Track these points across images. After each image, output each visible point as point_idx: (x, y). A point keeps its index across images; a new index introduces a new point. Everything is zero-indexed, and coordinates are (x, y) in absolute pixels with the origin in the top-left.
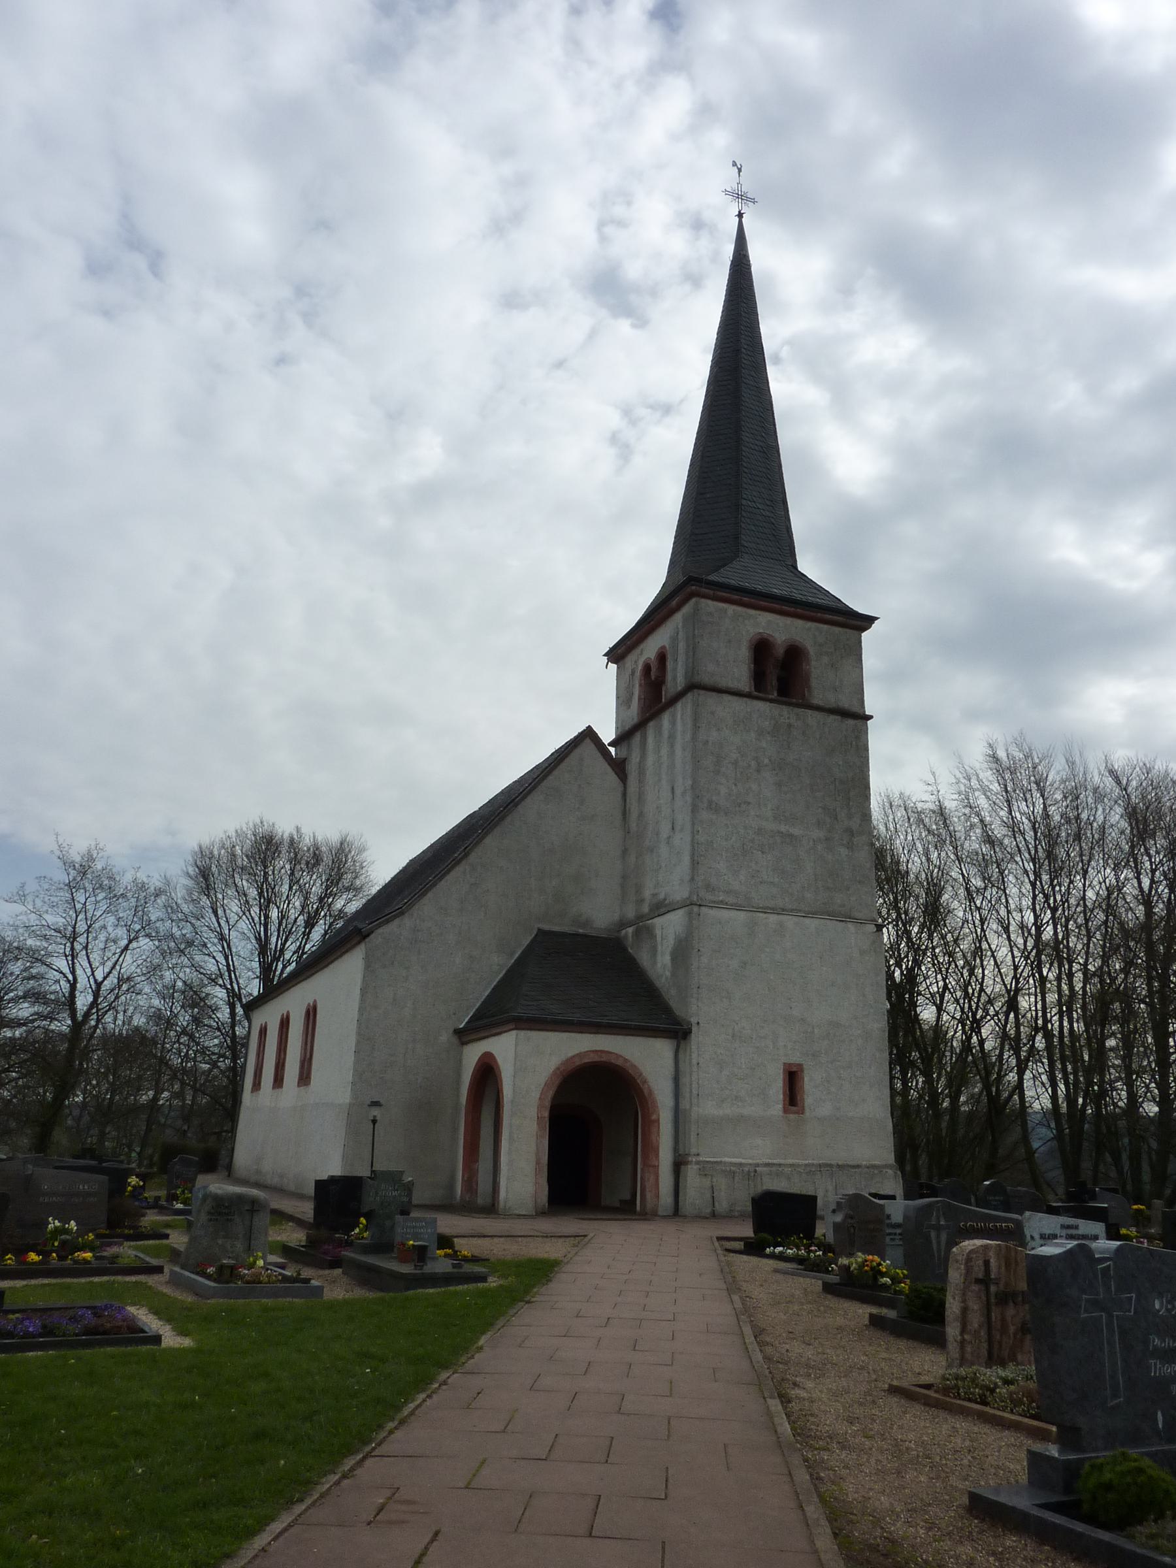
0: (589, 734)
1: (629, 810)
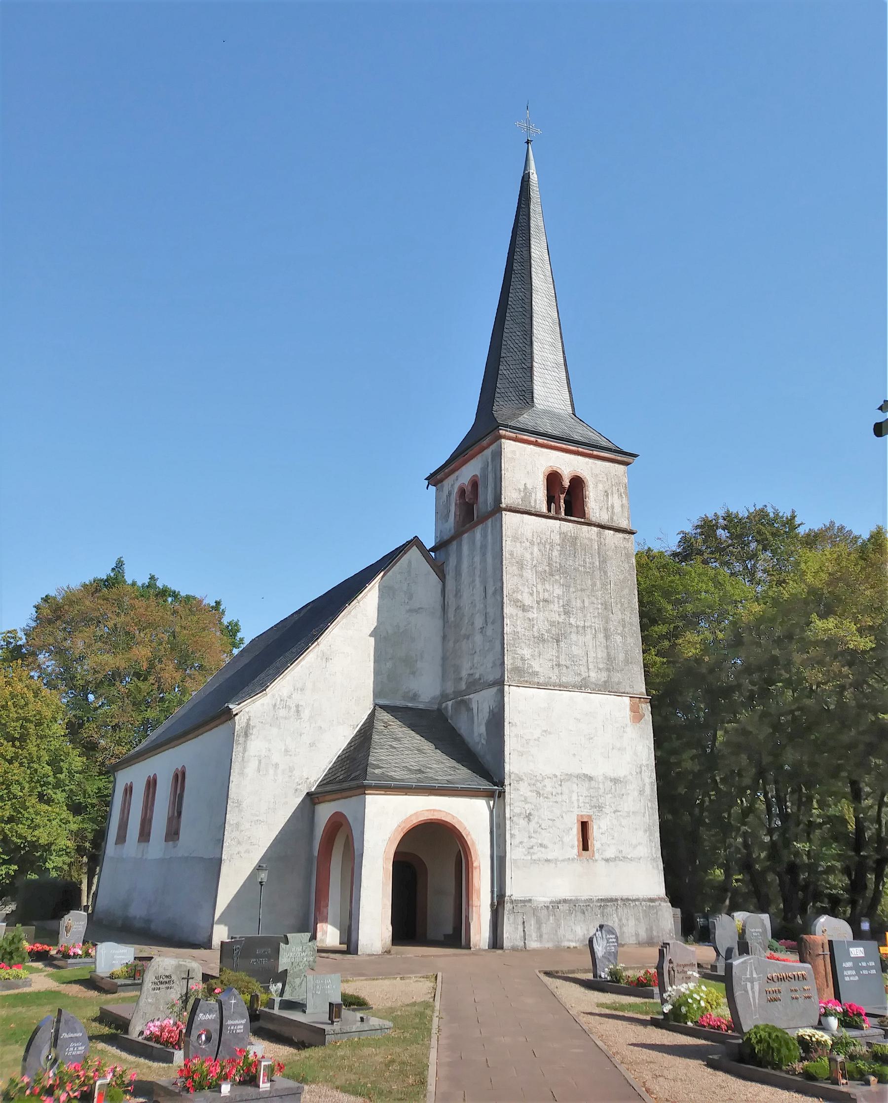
0: (415, 542)
1: (448, 605)
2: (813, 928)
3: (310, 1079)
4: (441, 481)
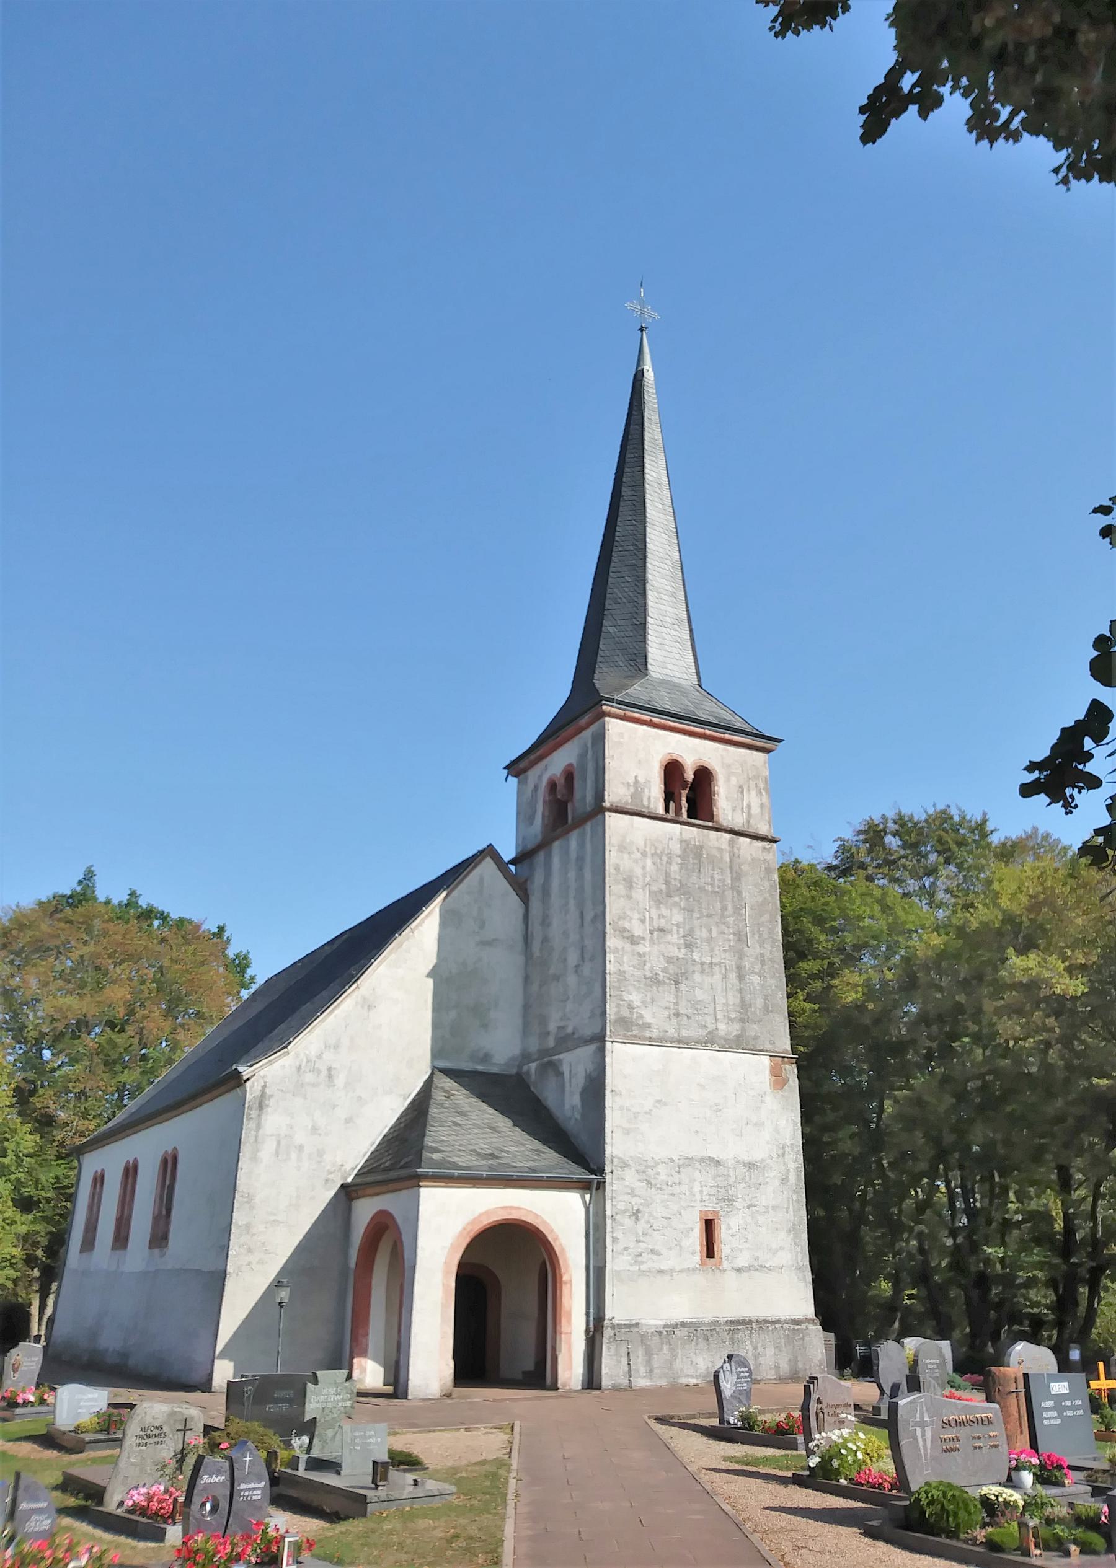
0: (490, 851)
2: (1006, 1358)
3: (347, 1560)
4: (525, 771)
